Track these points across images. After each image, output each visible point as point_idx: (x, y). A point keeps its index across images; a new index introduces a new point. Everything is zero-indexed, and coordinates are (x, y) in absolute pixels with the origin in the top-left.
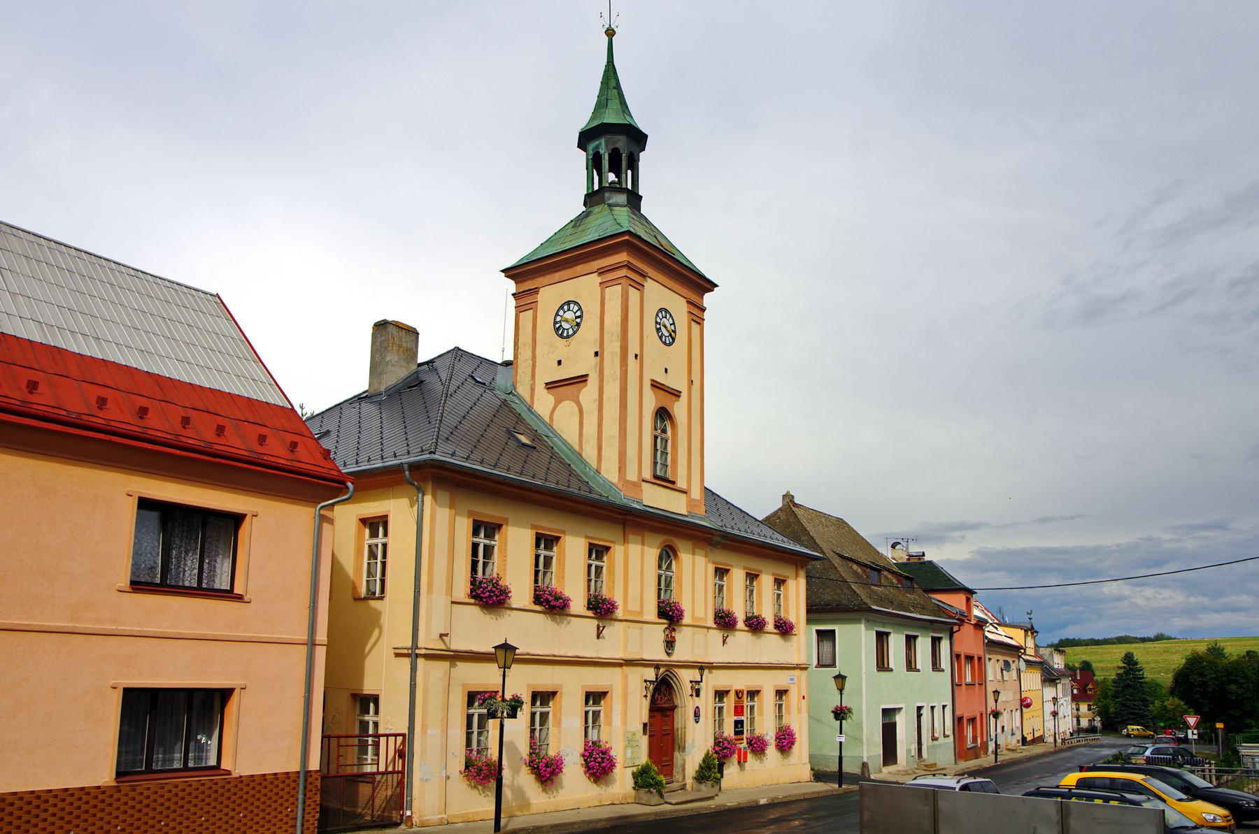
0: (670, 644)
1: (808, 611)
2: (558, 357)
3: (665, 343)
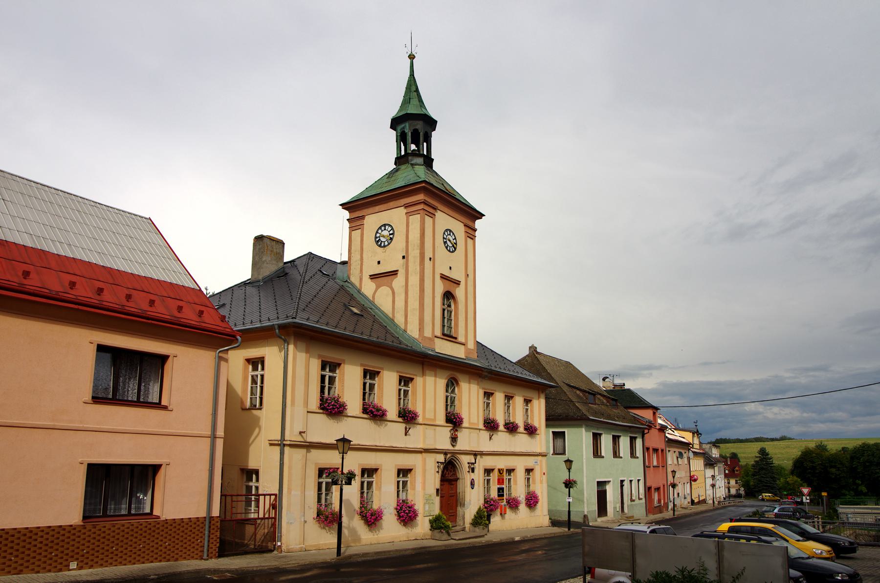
0: (454, 439)
1: (547, 420)
2: (374, 259)
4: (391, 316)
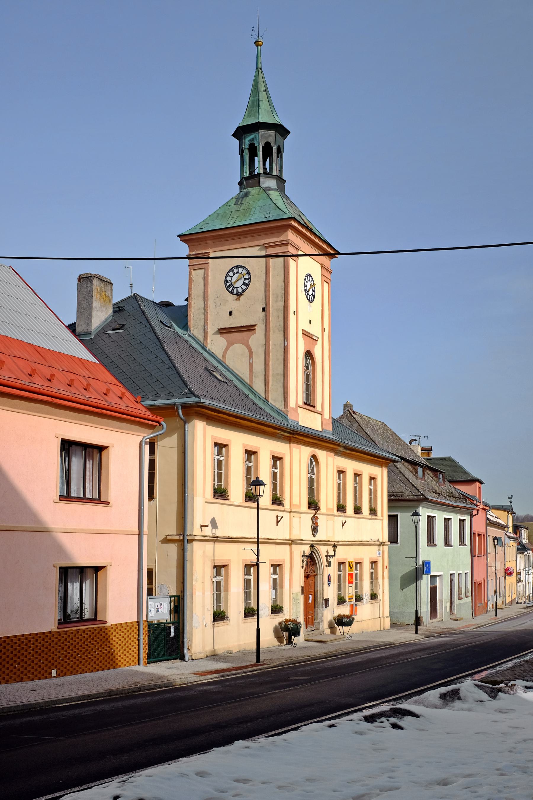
0: (315, 529)
1: (389, 501)
3: (309, 300)
4: (248, 381)
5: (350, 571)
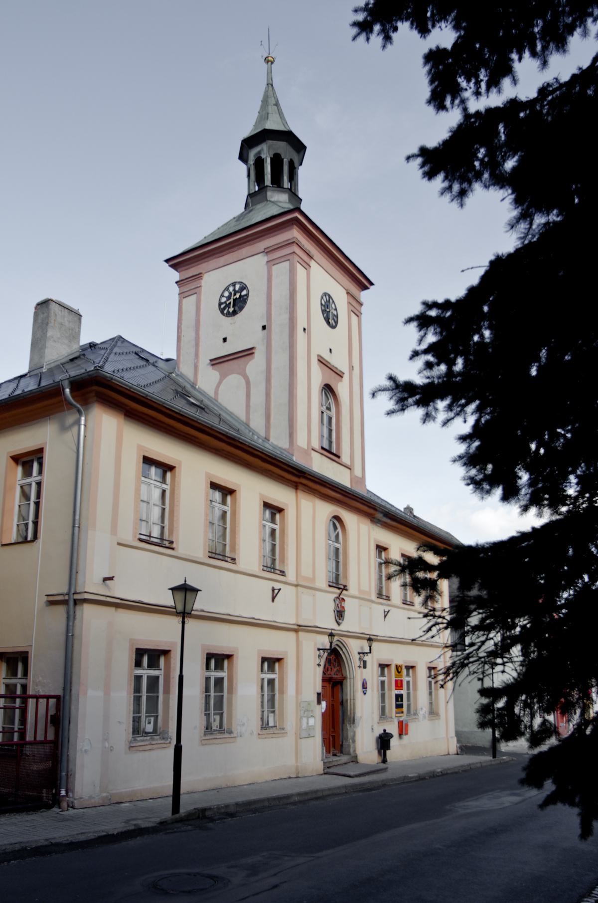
0: (340, 614)
2: (222, 333)
5: (397, 675)
